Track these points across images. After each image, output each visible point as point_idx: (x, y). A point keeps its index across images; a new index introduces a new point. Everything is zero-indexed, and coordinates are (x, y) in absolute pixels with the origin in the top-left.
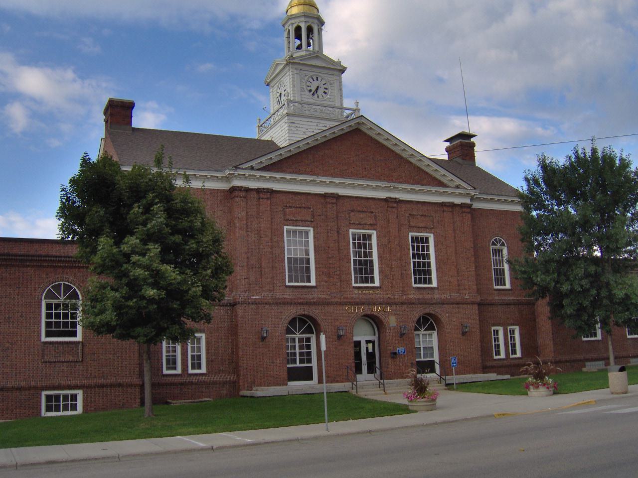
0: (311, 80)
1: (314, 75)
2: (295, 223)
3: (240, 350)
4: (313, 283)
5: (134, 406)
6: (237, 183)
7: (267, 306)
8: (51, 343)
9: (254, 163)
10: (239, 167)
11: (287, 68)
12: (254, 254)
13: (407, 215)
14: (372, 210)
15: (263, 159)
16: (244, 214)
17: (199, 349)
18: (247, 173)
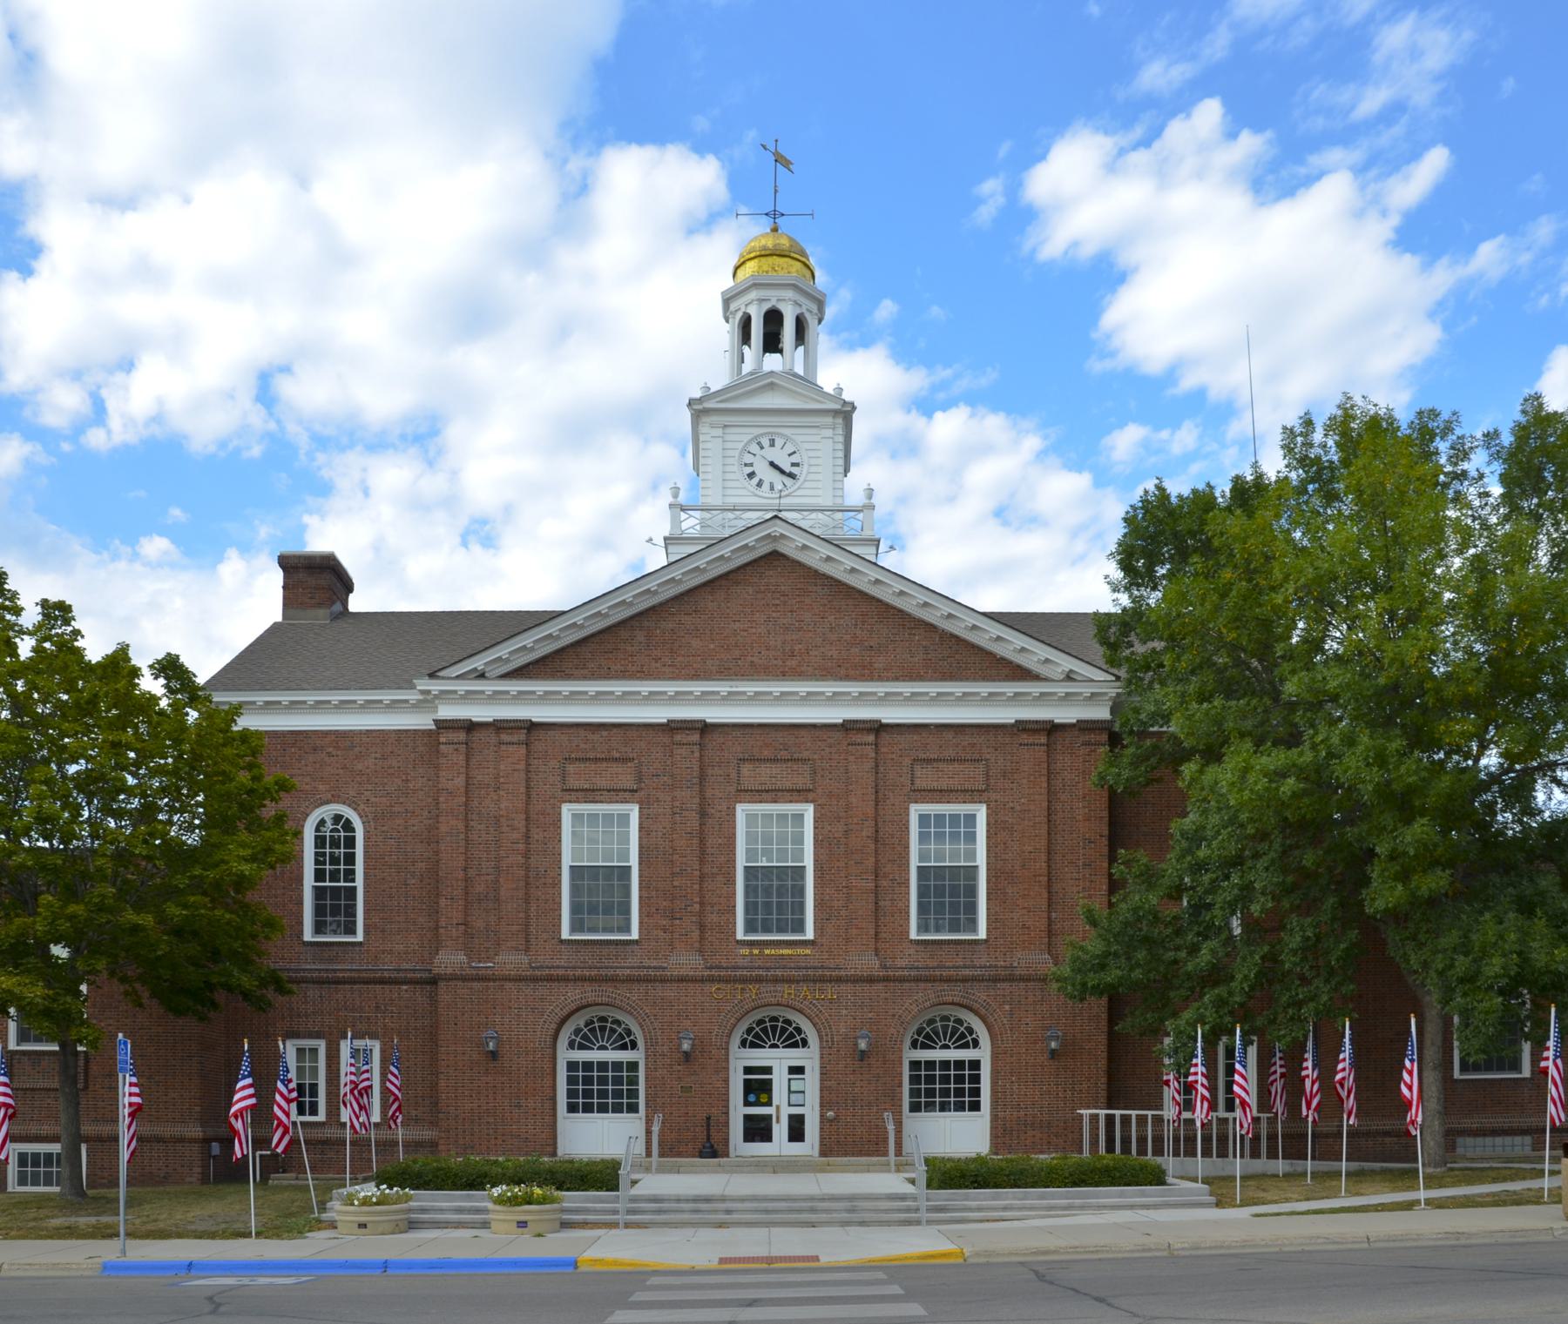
0: (754, 448)
1: (762, 435)
2: (590, 794)
3: (442, 1076)
4: (635, 935)
5: (188, 1179)
6: (447, 712)
7: (508, 985)
8: (24, 1053)
9: (478, 663)
10: (1114, 679)
11: (829, 420)
12: (484, 871)
13: (907, 761)
14: (805, 755)
15: (503, 651)
16: (460, 781)
17: (314, 1070)
18: (462, 687)
